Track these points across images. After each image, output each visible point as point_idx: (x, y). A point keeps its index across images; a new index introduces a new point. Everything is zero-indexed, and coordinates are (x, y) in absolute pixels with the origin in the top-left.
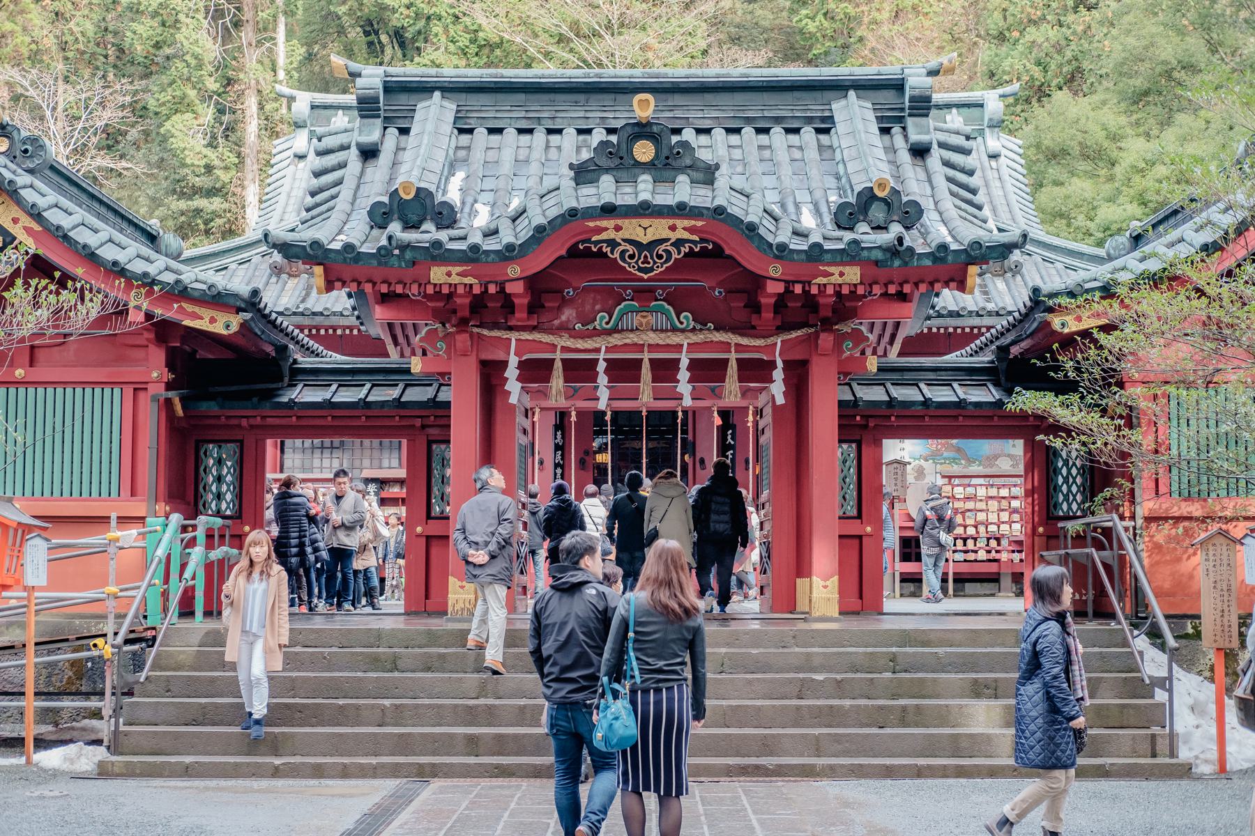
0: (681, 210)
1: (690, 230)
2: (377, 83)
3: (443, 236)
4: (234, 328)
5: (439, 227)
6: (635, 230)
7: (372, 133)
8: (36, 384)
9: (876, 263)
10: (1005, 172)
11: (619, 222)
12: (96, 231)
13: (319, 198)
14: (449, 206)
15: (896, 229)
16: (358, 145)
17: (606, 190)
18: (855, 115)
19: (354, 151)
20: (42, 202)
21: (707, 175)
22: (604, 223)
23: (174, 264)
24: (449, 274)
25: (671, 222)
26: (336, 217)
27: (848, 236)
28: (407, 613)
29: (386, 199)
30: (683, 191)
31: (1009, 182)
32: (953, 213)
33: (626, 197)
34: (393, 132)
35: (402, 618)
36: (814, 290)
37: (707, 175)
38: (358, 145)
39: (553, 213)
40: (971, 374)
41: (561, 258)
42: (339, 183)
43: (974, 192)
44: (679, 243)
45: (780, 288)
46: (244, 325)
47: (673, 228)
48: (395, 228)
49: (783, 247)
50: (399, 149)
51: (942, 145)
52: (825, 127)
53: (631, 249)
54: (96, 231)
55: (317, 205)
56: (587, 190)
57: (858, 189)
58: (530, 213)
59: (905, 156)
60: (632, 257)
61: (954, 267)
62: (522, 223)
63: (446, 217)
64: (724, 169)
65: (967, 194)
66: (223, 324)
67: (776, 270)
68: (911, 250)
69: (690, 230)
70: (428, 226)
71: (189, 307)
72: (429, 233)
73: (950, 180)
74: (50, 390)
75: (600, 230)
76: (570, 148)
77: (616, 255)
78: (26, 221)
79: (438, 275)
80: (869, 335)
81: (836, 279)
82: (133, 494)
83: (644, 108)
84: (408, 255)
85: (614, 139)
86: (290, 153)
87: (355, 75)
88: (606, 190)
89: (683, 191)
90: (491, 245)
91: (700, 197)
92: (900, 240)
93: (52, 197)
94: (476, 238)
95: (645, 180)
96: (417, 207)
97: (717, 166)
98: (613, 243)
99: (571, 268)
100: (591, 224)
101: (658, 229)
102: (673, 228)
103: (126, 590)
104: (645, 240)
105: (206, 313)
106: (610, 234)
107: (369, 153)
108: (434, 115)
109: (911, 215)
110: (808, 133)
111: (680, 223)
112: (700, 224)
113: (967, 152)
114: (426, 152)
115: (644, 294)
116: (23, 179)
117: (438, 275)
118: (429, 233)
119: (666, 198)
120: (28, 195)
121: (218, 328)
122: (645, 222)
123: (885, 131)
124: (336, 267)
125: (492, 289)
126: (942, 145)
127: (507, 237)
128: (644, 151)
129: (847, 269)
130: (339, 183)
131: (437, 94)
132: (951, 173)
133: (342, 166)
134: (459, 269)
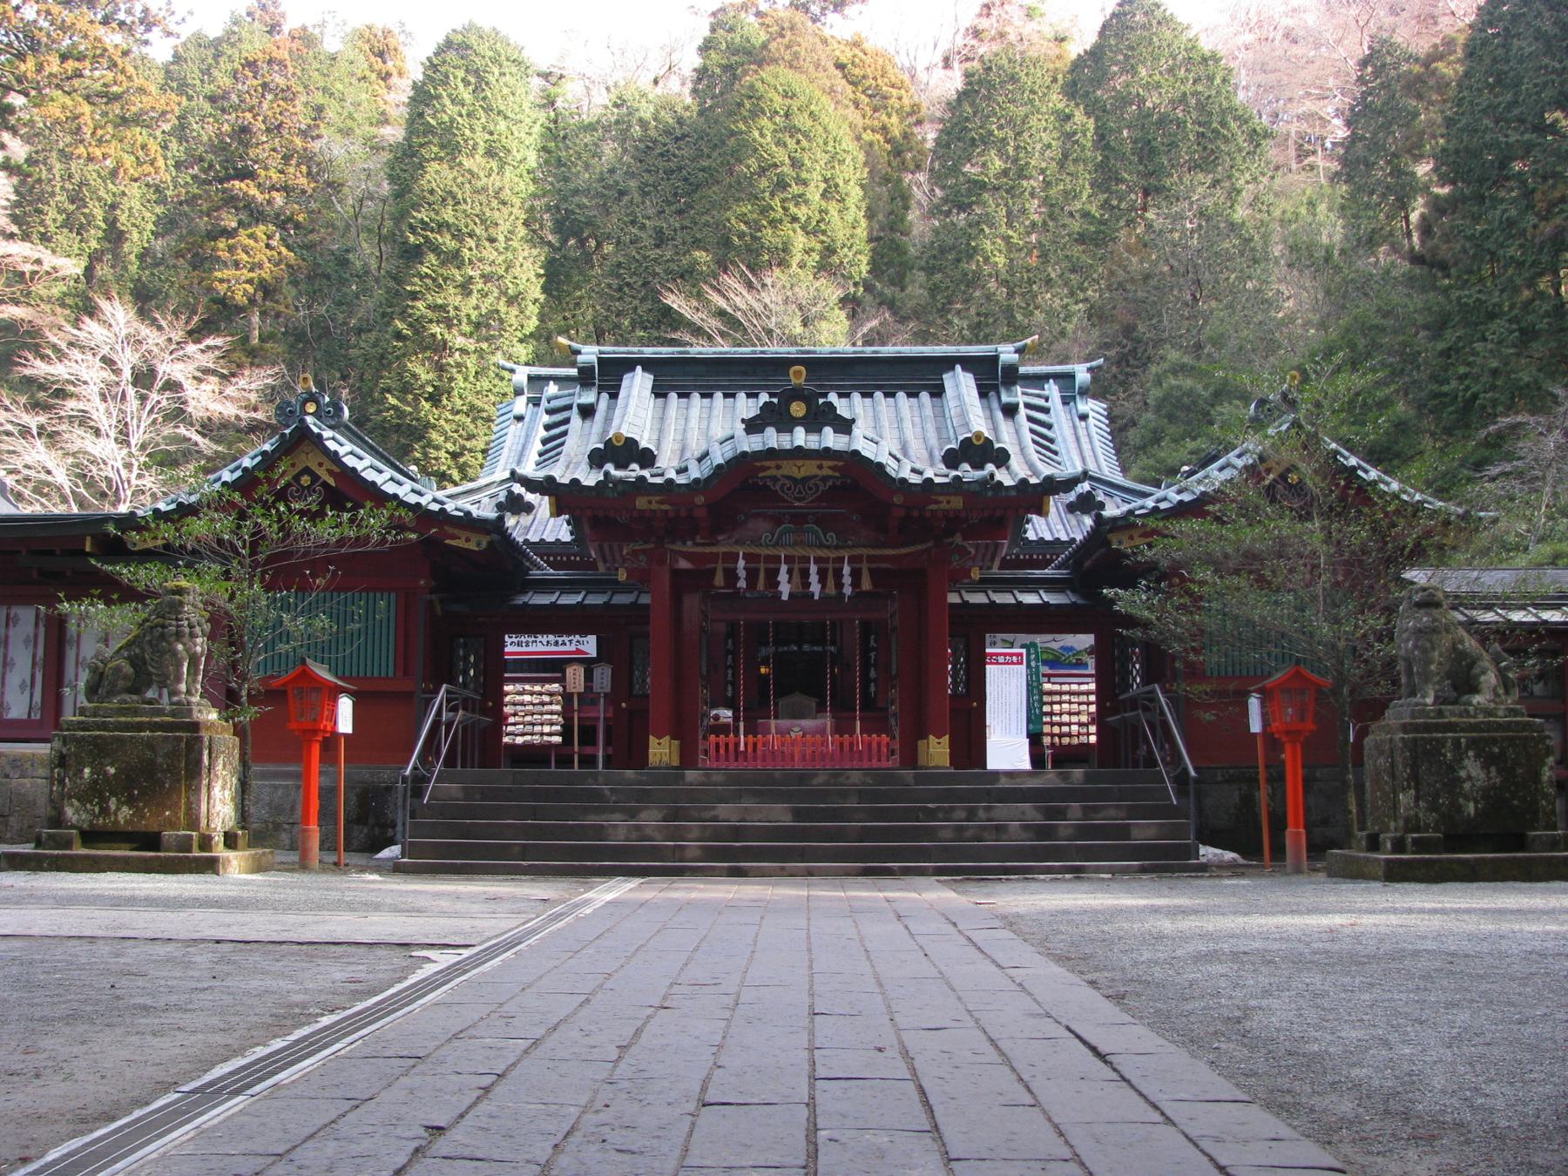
3: (646, 473)
4: (484, 545)
5: (642, 467)
7: (589, 397)
10: (1093, 430)
12: (380, 472)
14: (647, 450)
15: (990, 467)
16: (579, 406)
17: (772, 438)
18: (961, 385)
19: (575, 409)
22: (768, 464)
27: (954, 473)
29: (601, 446)
30: (830, 439)
31: (1096, 437)
32: (1035, 457)
34: (605, 396)
37: (844, 426)
40: (1051, 585)
43: (1052, 441)
44: (825, 479)
46: (490, 544)
48: (609, 467)
52: (938, 392)
53: (788, 483)
54: (380, 472)
57: (961, 438)
59: (999, 415)
61: (1033, 497)
62: (707, 463)
63: (648, 458)
64: (859, 422)
65: (1046, 444)
68: (1000, 483)
70: (634, 466)
71: (449, 530)
72: (634, 471)
73: (1032, 431)
75: (765, 469)
76: (747, 407)
77: (778, 488)
78: (328, 465)
80: (997, 563)
81: (944, 506)
82: (405, 673)
83: (798, 376)
84: (620, 488)
85: (775, 400)
86: (510, 415)
88: (772, 438)
89: (830, 439)
90: (681, 480)
92: (992, 476)
94: (672, 474)
95: (800, 432)
96: (624, 451)
97: (853, 421)
98: (774, 479)
101: (809, 468)
102: (820, 467)
104: (799, 476)
105: (464, 534)
106: (773, 472)
108: (638, 384)
109: (1002, 458)
110: (924, 396)
111: (825, 463)
114: (637, 411)
115: (799, 519)
116: (327, 433)
117: (641, 503)
118: (634, 471)
121: (472, 546)
122: (800, 463)
124: (565, 497)
126: (1027, 406)
127: (695, 473)
128: (798, 409)
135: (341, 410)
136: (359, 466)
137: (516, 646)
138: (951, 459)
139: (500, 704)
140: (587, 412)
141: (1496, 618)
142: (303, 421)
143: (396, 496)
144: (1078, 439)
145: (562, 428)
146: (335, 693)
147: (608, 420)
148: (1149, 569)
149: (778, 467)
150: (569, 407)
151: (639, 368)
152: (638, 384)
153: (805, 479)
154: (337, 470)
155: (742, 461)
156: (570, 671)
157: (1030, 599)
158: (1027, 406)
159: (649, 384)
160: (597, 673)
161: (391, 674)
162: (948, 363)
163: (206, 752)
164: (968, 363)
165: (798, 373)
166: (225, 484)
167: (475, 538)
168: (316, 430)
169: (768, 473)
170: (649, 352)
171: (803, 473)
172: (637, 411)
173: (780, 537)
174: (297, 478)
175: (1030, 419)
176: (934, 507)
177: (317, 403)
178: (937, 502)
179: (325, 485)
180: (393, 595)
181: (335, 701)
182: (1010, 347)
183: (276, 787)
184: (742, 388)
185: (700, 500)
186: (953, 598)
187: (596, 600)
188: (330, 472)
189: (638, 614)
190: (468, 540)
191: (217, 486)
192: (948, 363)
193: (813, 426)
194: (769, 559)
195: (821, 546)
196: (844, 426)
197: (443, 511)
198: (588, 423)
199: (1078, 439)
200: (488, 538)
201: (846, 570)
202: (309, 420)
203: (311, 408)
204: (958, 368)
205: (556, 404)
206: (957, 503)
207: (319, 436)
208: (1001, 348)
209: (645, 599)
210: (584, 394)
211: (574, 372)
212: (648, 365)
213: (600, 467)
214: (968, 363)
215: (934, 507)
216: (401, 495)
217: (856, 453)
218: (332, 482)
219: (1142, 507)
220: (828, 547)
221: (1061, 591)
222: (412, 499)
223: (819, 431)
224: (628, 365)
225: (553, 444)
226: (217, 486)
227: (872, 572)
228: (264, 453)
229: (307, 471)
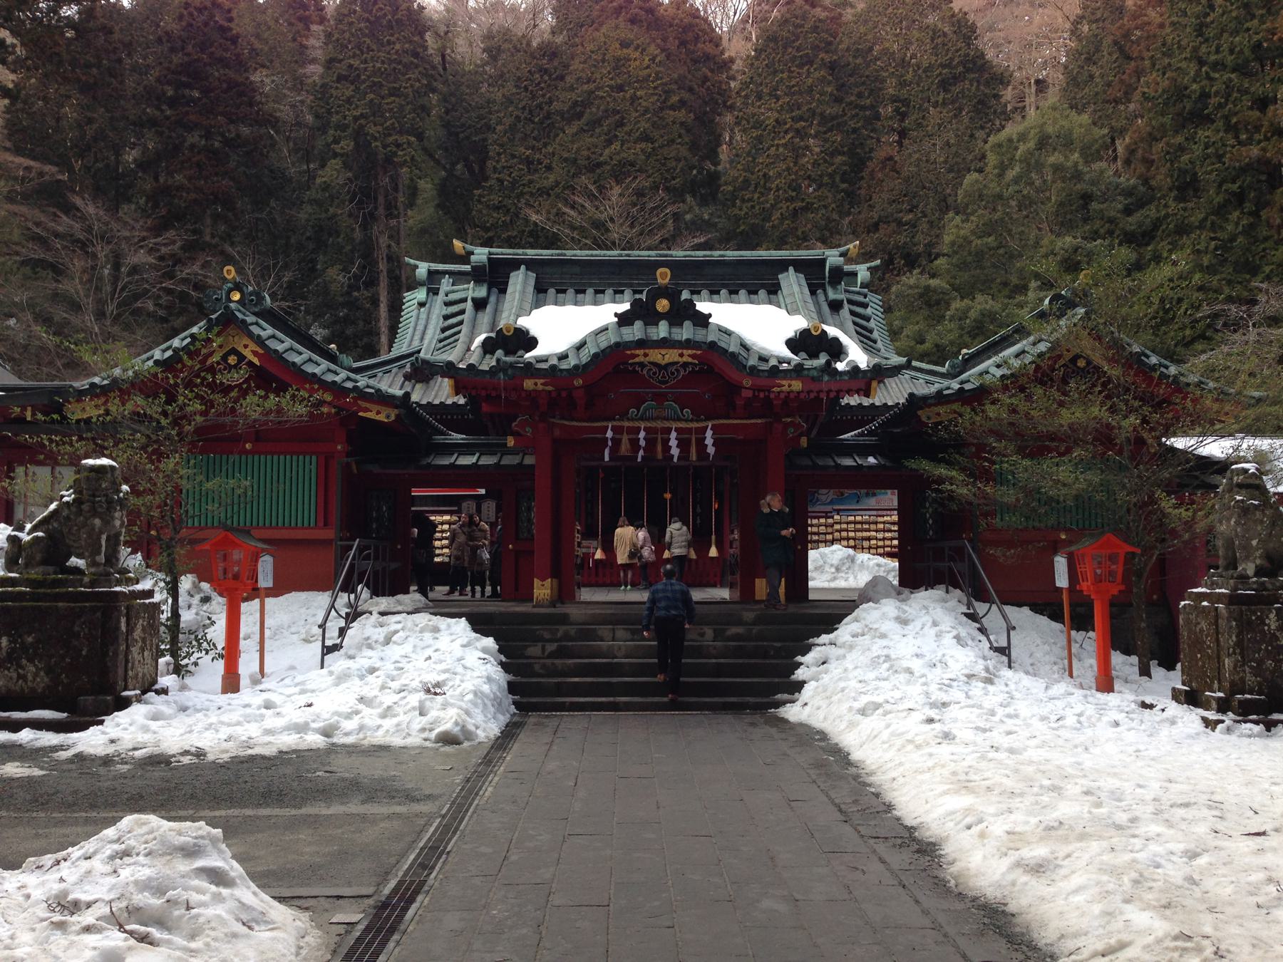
0: (688, 344)
2: (484, 258)
4: (393, 418)
6: (656, 356)
8: (260, 453)
9: (813, 379)
13: (448, 333)
17: (636, 331)
19: (470, 302)
20: (264, 334)
22: (637, 352)
23: (352, 375)
26: (460, 347)
30: (686, 331)
36: (772, 396)
38: (473, 299)
39: (604, 345)
42: (461, 323)
44: (685, 365)
45: (749, 394)
46: (397, 416)
47: (681, 355)
49: (753, 368)
50: (498, 301)
58: (589, 344)
66: (382, 415)
67: (747, 382)
71: (363, 404)
73: (855, 323)
79: (528, 384)
81: (786, 388)
82: (326, 525)
86: (415, 301)
91: (700, 335)
93: (270, 331)
98: (642, 365)
101: (671, 356)
103: (424, 333)
104: (663, 363)
105: (375, 408)
106: (641, 359)
108: (519, 282)
113: (865, 306)
117: (528, 384)
120: (255, 330)
121: (381, 417)
122: (663, 352)
123: (813, 293)
125: (564, 394)
126: (850, 302)
129: (793, 382)
132: (857, 320)
133: (462, 312)
142: (227, 308)
144: (426, 327)
145: (459, 318)
147: (496, 312)
148: (958, 444)
150: (464, 300)
151: (523, 267)
155: (618, 347)
156: (464, 505)
158: (850, 302)
159: (532, 282)
160: (484, 506)
162: (783, 265)
163: (123, 620)
164: (800, 265)
165: (663, 275)
166: (156, 362)
170: (531, 253)
171: (668, 359)
174: (225, 358)
175: (853, 313)
179: (250, 364)
180: (314, 458)
182: (835, 252)
185: (578, 382)
187: (487, 460)
189: (523, 471)
190: (378, 413)
191: (150, 363)
192: (783, 265)
195: (679, 419)
199: (426, 327)
200: (396, 411)
205: (452, 297)
206: (797, 385)
208: (828, 252)
209: (529, 460)
210: (477, 289)
211: (467, 268)
212: (531, 264)
213: (493, 353)
214: (800, 265)
218: (256, 361)
219: (948, 388)
220: (686, 421)
223: (681, 325)
224: (514, 264)
225: (449, 332)
226: (150, 363)
228: (192, 336)
229: (234, 351)
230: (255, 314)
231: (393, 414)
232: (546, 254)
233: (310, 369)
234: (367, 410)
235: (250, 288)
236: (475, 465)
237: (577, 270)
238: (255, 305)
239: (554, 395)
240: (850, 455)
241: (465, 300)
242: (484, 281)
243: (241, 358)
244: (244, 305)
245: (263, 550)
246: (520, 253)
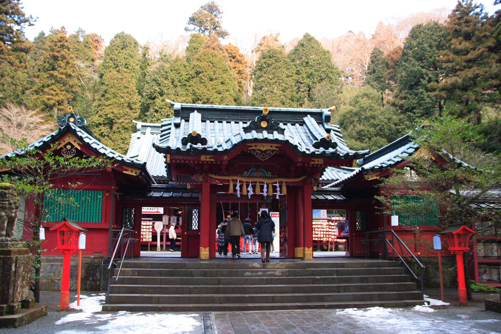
1: (276, 147)
4: (138, 174)
7: (178, 120)
11: (256, 144)
12: (98, 145)
17: (254, 135)
19: (173, 125)
21: (282, 131)
22: (252, 144)
24: (206, 158)
25: (271, 145)
28: (182, 257)
30: (276, 135)
33: (260, 136)
34: (183, 121)
35: (180, 259)
41: (238, 155)
44: (273, 151)
45: (300, 165)
51: (334, 130)
53: (259, 152)
54: (98, 145)
55: (163, 139)
56: (248, 134)
60: (260, 154)
63: (204, 141)
69: (276, 147)
71: (125, 168)
72: (199, 146)
74: (90, 192)
78: (78, 141)
79: (203, 158)
82: (105, 222)
87: (173, 105)
89: (276, 135)
91: (280, 137)
95: (265, 133)
96: (195, 138)
98: (254, 150)
99: (241, 157)
100: (248, 145)
102: (272, 146)
105: (130, 169)
107: (177, 126)
108: (195, 117)
111: (274, 145)
112: (279, 145)
116: (78, 129)
117: (203, 158)
118: (199, 146)
119: (270, 137)
122: (264, 144)
126: (334, 130)
128: (264, 124)
129: (320, 160)
130: (169, 133)
131: (196, 111)
133: (170, 129)
134: (209, 156)
135: (84, 121)
136: (90, 142)
137: (145, 210)
138: (316, 146)
139: (140, 231)
140: (177, 126)
141: (317, 196)
142: (68, 124)
143: (104, 154)
146: (78, 232)
149: (256, 146)
151: (196, 111)
152: (195, 117)
153: (266, 151)
154: (81, 143)
157: (330, 198)
161: (100, 222)
163: (13, 265)
164: (312, 114)
167: (134, 171)
168: (73, 128)
169: (252, 148)
172: (195, 124)
173: (250, 173)
174: (65, 146)
176: (313, 163)
177: (74, 118)
178: (314, 161)
179: (76, 149)
181: (78, 236)
183: (52, 265)
184: (233, 120)
186: (313, 197)
188: (79, 144)
190: (132, 171)
192: (192, 110)
193: (270, 130)
194: (233, 180)
196: (282, 131)
197: (123, 160)
198: (178, 130)
201: (238, 185)
202: (71, 124)
203: (72, 120)
204: (309, 116)
207: (75, 130)
212: (199, 110)
215: (313, 163)
216: (106, 153)
217: (287, 141)
218: (79, 148)
221: (339, 195)
222: (111, 155)
223: (272, 133)
227: (287, 186)
230: (79, 127)
231: (138, 172)
232: (206, 106)
233: (94, 146)
234: (126, 170)
235: (78, 117)
236: (181, 196)
237: (219, 113)
238: (80, 124)
239: (214, 163)
240: (330, 195)
241: (170, 124)
242: (179, 116)
243: (73, 146)
244: (75, 124)
245: (82, 231)
246: (194, 105)
